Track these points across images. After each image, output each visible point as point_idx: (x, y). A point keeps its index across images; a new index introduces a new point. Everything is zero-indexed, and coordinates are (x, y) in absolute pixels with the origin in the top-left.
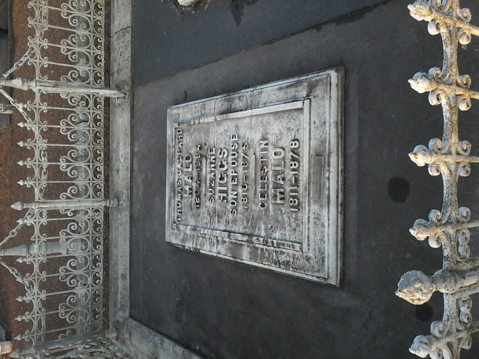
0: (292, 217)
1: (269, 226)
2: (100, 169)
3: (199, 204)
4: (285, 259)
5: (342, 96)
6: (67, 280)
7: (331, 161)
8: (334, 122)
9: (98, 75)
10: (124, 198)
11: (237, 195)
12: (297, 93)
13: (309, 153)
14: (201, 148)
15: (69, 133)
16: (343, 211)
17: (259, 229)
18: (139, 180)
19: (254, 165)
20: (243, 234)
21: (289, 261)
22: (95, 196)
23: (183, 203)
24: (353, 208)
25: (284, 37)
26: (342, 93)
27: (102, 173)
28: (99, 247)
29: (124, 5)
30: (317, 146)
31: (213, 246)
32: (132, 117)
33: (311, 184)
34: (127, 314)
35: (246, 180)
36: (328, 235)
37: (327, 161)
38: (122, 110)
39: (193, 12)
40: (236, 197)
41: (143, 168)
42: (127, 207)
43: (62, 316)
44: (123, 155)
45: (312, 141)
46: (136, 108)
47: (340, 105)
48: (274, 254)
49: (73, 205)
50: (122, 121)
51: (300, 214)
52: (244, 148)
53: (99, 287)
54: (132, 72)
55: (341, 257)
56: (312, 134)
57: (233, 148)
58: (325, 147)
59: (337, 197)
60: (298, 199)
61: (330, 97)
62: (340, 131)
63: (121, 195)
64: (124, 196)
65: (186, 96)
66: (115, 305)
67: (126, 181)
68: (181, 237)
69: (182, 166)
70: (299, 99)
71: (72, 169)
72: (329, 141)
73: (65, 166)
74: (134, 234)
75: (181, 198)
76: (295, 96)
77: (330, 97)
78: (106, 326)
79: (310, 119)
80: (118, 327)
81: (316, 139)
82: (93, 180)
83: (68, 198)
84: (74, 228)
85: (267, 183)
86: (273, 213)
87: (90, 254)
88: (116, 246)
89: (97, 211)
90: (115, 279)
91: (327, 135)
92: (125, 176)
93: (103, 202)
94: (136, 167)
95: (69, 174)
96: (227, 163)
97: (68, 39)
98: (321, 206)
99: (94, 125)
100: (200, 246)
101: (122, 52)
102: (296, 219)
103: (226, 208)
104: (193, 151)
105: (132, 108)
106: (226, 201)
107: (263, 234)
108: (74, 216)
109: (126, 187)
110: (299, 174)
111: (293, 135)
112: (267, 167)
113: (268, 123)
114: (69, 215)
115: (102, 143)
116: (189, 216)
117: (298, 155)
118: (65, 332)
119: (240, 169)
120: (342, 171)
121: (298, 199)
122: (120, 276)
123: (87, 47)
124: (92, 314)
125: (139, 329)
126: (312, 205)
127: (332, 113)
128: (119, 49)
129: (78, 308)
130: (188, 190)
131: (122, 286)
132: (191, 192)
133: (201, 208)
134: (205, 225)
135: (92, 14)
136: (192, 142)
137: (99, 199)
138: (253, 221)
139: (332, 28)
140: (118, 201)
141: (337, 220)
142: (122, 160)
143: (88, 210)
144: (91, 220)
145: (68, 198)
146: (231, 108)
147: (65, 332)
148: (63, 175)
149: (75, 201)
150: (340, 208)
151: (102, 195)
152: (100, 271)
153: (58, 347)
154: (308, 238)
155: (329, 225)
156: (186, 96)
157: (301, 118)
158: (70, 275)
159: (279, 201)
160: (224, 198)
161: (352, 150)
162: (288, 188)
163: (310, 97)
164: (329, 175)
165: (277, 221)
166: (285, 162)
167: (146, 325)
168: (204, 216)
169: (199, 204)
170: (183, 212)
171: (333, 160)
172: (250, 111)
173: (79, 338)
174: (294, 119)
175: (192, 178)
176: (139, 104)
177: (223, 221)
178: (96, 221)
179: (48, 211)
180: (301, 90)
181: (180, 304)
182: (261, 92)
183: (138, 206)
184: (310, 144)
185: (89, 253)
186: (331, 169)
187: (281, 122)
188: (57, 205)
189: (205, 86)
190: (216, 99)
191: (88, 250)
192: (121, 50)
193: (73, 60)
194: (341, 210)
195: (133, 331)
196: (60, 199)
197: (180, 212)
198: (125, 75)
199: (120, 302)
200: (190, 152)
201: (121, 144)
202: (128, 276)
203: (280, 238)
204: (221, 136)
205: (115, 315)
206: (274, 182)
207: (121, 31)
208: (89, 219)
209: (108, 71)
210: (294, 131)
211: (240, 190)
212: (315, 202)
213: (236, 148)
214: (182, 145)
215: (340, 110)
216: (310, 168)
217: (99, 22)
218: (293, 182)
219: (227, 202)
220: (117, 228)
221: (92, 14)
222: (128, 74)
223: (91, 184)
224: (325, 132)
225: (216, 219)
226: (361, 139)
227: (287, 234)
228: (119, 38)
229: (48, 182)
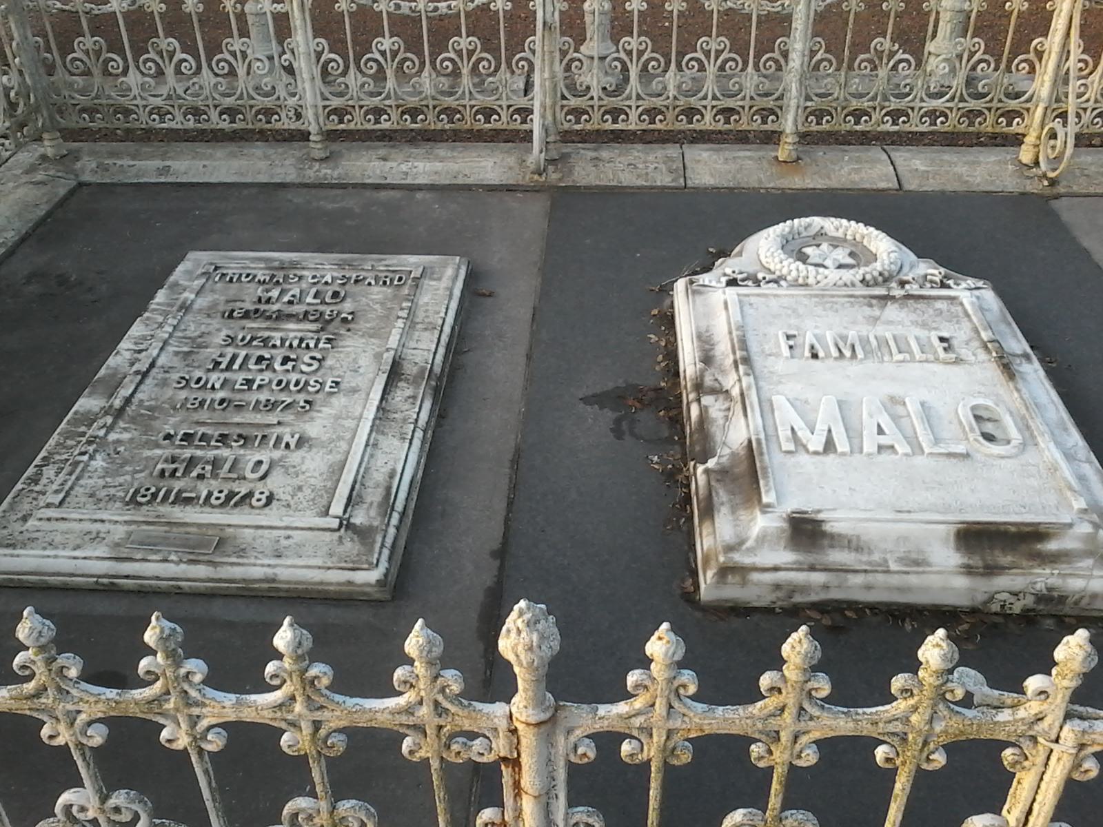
0: (118, 491)
1: (121, 449)
2: (385, 120)
3: (231, 316)
4: (45, 476)
5: (327, 592)
6: (152, 55)
7: (198, 566)
8: (275, 574)
9: (660, 117)
10: (324, 171)
11: (213, 388)
12: (365, 506)
13: (229, 526)
14: (345, 320)
15: (452, 55)
16: (102, 588)
17: (125, 429)
18: (352, 202)
19: (256, 421)
20: (128, 401)
21: (36, 484)
22: (327, 110)
23: (248, 285)
24: (102, 606)
25: (514, 488)
26: (335, 592)
27: (378, 126)
28: (225, 120)
29: (740, 170)
30: (239, 541)
31: (136, 344)
32: (492, 189)
33: (166, 528)
34: (87, 177)
35: (236, 406)
36: (56, 557)
37: (201, 558)
38: (510, 168)
39: (655, 312)
40: (209, 386)
41: (373, 208)
42: (304, 176)
43: (227, 44)
44: (415, 170)
45: (252, 531)
46: (508, 197)
47: (309, 587)
48: (65, 456)
49: (303, 66)
50: (487, 166)
51: (118, 504)
52: (302, 404)
53: (144, 120)
54: (585, 187)
55: (12, 580)
56: (267, 531)
57: (312, 383)
58: (229, 556)
59: (127, 577)
60: (149, 502)
61: (329, 568)
62: (256, 586)
63: (332, 165)
64: (329, 171)
65: (484, 295)
66: (113, 154)
67: (358, 175)
68: (181, 282)
69: (326, 283)
70: (349, 509)
71: (776, 61)
72: (239, 564)
73: (382, 48)
74: (245, 192)
75: (259, 281)
76: (361, 500)
77: (329, 568)
78: (70, 135)
79: (297, 528)
80: (62, 159)
81: (254, 539)
82: (361, 107)
83: (319, 55)
84: (332, 68)
85: (209, 445)
86: (144, 455)
87: (210, 102)
88: (233, 155)
89: (299, 116)
90: (166, 153)
91: (252, 561)
92: (369, 172)
93: (317, 127)
94: (383, 195)
95: (768, 56)
96: (288, 371)
97: (984, 53)
98: (117, 545)
99: (476, 108)
100: (148, 319)
101: (636, 167)
102: (111, 498)
103: (199, 367)
104: (348, 306)
105: (510, 189)
106: (211, 367)
107: (112, 437)
108: (284, 67)
109: (346, 174)
110: (198, 507)
111: (282, 496)
112: (241, 446)
113: (331, 451)
114: (284, 57)
115: (439, 126)
116: (216, 296)
117: (236, 505)
118: (49, 50)
119: (263, 396)
120: (179, 588)
121: (149, 502)
122: (168, 163)
123: (640, 92)
124: (89, 104)
125: (45, 200)
126: (126, 528)
127: (304, 571)
128: (645, 162)
129: (97, 79)
130: (270, 294)
131: (146, 167)
132: (263, 300)
133: (222, 320)
134: (183, 327)
135: (714, 103)
136: (368, 305)
137: (321, 120)
138: (145, 421)
139: (488, 579)
140: (322, 160)
141: (82, 576)
142: (404, 167)
143: (297, 97)
144: (278, 103)
145: (319, 55)
146: (401, 380)
147: (49, 50)
148: (439, 45)
149: (312, 69)
150: (105, 581)
151: (330, 127)
152: (177, 122)
153: (16, 35)
154: (63, 519)
155: (75, 558)
156: (484, 295)
157: (308, 512)
158: (386, 60)
159: (160, 466)
160: (217, 364)
161: (218, 609)
162: (177, 485)
163: (343, 530)
164: (172, 561)
165: (126, 462)
166: (234, 480)
167: (49, 214)
168: (203, 326)
169: (231, 316)
170: (231, 285)
171: (201, 571)
172: (371, 416)
173: (37, 78)
174: (313, 500)
175: (290, 302)
176: (511, 201)
177: (176, 362)
178: (277, 113)
179: (287, 13)
180: (368, 514)
181: (63, 281)
182: (404, 439)
183: (298, 198)
184: (247, 526)
185: (210, 99)
186: (183, 566)
187: (321, 474)
188: (300, 32)
189: (487, 333)
190: (435, 353)
191: (217, 96)
192: (641, 166)
193: (860, 64)
194: (103, 585)
195: (44, 189)
196: (315, 37)
197: (231, 279)
198: (583, 173)
199: (115, 164)
200: (349, 300)
201: (438, 164)
202: (163, 180)
203: (89, 468)
204: (351, 359)
205: (92, 153)
206: (202, 458)
207: (681, 165)
208: (279, 98)
209: (585, 137)
210: (289, 498)
211: (221, 395)
212: (129, 534)
213: (310, 389)
214: (370, 284)
215: (300, 587)
216: (199, 526)
217: (698, 117)
218: (184, 495)
219: (209, 370)
220: (267, 157)
221: (714, 103)
222: (584, 181)
223: (350, 103)
224: (260, 556)
225: (186, 349)
226: (230, 625)
227: (91, 481)
228: (670, 159)
229: (345, 13)
